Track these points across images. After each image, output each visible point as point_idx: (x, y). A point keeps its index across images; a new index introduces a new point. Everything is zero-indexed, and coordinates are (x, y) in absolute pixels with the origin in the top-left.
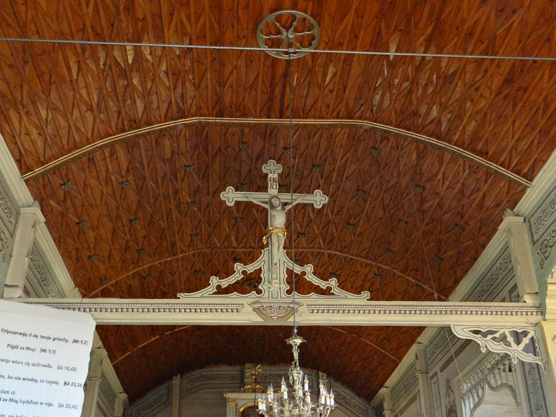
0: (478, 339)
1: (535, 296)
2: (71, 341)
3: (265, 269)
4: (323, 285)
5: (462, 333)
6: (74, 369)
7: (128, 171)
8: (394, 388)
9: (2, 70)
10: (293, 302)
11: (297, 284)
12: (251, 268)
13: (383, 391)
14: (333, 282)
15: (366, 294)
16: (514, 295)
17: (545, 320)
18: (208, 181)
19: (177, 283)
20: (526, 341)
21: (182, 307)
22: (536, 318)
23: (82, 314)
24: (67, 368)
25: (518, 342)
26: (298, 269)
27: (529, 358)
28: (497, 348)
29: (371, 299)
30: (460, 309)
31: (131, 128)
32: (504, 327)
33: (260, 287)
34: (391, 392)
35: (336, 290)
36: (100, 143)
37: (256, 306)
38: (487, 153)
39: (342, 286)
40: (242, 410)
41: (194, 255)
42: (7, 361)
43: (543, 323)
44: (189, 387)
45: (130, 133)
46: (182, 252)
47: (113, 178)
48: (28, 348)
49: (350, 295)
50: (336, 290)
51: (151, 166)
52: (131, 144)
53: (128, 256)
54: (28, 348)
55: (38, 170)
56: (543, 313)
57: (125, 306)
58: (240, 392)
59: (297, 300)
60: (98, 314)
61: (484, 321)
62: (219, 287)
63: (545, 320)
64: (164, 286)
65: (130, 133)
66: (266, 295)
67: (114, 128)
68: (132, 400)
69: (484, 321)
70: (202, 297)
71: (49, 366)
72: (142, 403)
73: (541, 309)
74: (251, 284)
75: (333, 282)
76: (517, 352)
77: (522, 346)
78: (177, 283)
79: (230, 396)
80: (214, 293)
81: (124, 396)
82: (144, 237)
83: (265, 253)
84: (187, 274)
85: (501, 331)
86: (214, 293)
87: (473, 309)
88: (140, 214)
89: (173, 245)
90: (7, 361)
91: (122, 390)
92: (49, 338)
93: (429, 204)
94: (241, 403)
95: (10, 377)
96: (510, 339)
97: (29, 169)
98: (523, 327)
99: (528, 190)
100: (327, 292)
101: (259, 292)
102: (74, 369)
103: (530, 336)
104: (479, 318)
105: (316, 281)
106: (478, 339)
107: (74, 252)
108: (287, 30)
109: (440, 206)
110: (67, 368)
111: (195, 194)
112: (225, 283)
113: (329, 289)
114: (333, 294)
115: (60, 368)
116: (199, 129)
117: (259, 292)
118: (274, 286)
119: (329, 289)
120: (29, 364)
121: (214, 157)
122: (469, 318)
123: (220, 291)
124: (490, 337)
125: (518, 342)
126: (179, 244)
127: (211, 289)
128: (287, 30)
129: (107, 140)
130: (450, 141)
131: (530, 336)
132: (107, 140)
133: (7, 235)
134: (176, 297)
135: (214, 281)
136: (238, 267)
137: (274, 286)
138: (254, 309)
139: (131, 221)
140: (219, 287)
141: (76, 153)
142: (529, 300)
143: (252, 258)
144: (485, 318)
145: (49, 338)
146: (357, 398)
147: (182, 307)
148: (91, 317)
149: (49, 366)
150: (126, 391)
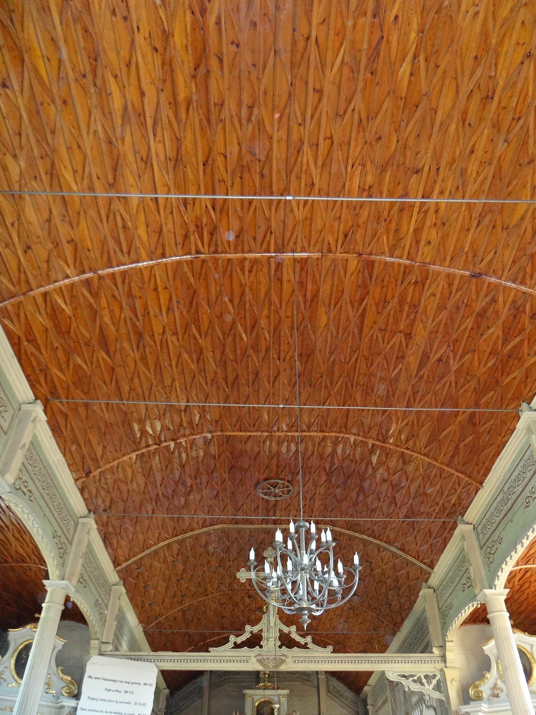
0: (403, 681)
1: (439, 649)
2: (142, 684)
3: (265, 629)
4: (302, 641)
5: (392, 677)
6: (144, 705)
7: (178, 554)
8: (375, 687)
9: (5, 169)
10: (283, 655)
11: (287, 641)
12: (256, 629)
13: (366, 688)
14: (309, 639)
15: (330, 648)
16: (426, 649)
17: (446, 667)
18: (229, 554)
19: (208, 611)
20: (434, 682)
21: (212, 658)
22: (441, 665)
23: (149, 663)
24: (140, 704)
25: (429, 683)
26: (286, 630)
27: (436, 695)
28: (415, 687)
29: (334, 651)
30: (391, 659)
31: (181, 534)
32: (420, 672)
33: (261, 643)
34: (373, 689)
35: (311, 645)
36: (162, 544)
37: (259, 658)
38: (404, 550)
39: (314, 642)
40: (257, 704)
41: (220, 595)
42: (105, 700)
43: (445, 669)
44: (217, 681)
45: (180, 537)
46: (212, 593)
47: (168, 560)
48: (117, 691)
49: (320, 649)
50: (311, 645)
51: (193, 550)
52: (181, 542)
53: (175, 600)
54: (117, 691)
55: (124, 565)
56: (445, 662)
57: (176, 658)
58: (256, 689)
59: (286, 653)
60: (159, 664)
61: (407, 668)
62: (235, 643)
63: (446, 667)
64: (199, 614)
65: (180, 537)
66: (265, 649)
67: (170, 534)
68: (172, 693)
69: (407, 668)
70: (224, 650)
71: (129, 703)
72: (181, 694)
73: (443, 658)
74: (254, 641)
75: (309, 639)
76: (428, 689)
77: (432, 686)
78: (208, 611)
79: (248, 692)
80: (232, 648)
81: (167, 691)
82: (187, 588)
83: (265, 617)
84: (215, 606)
85: (418, 675)
86: (232, 648)
87: (400, 659)
88: (184, 575)
89: (206, 590)
90: (105, 700)
91: (165, 686)
92: (129, 683)
93: (377, 571)
94: (256, 698)
95: (106, 712)
96: (424, 681)
97: (119, 565)
98: (433, 672)
99: (432, 575)
100: (305, 647)
101: (261, 647)
102: (144, 705)
103: (437, 678)
104: (403, 665)
105: (298, 638)
106: (403, 681)
107: (140, 604)
108: (274, 487)
109: (383, 574)
110: (140, 704)
111: (221, 561)
112: (239, 640)
113: (306, 644)
114: (308, 648)
115: (136, 704)
116: (223, 531)
117: (261, 647)
118: (271, 642)
119: (306, 644)
120: (117, 702)
121: (233, 543)
122: (397, 665)
123: (237, 646)
124: (411, 679)
125: (429, 683)
126: (210, 589)
127: (230, 644)
128: (274, 487)
129: (166, 542)
130: (381, 540)
131: (437, 678)
132: (166, 542)
133: (104, 607)
134: (207, 651)
135: (232, 639)
136: (248, 628)
137: (271, 642)
138: (258, 660)
139: (178, 580)
140: (235, 643)
141: (147, 551)
142: (436, 651)
143: (257, 621)
144: (407, 665)
145: (129, 683)
146: (349, 691)
147: (212, 658)
148: (155, 667)
149: (129, 703)
150: (168, 686)
